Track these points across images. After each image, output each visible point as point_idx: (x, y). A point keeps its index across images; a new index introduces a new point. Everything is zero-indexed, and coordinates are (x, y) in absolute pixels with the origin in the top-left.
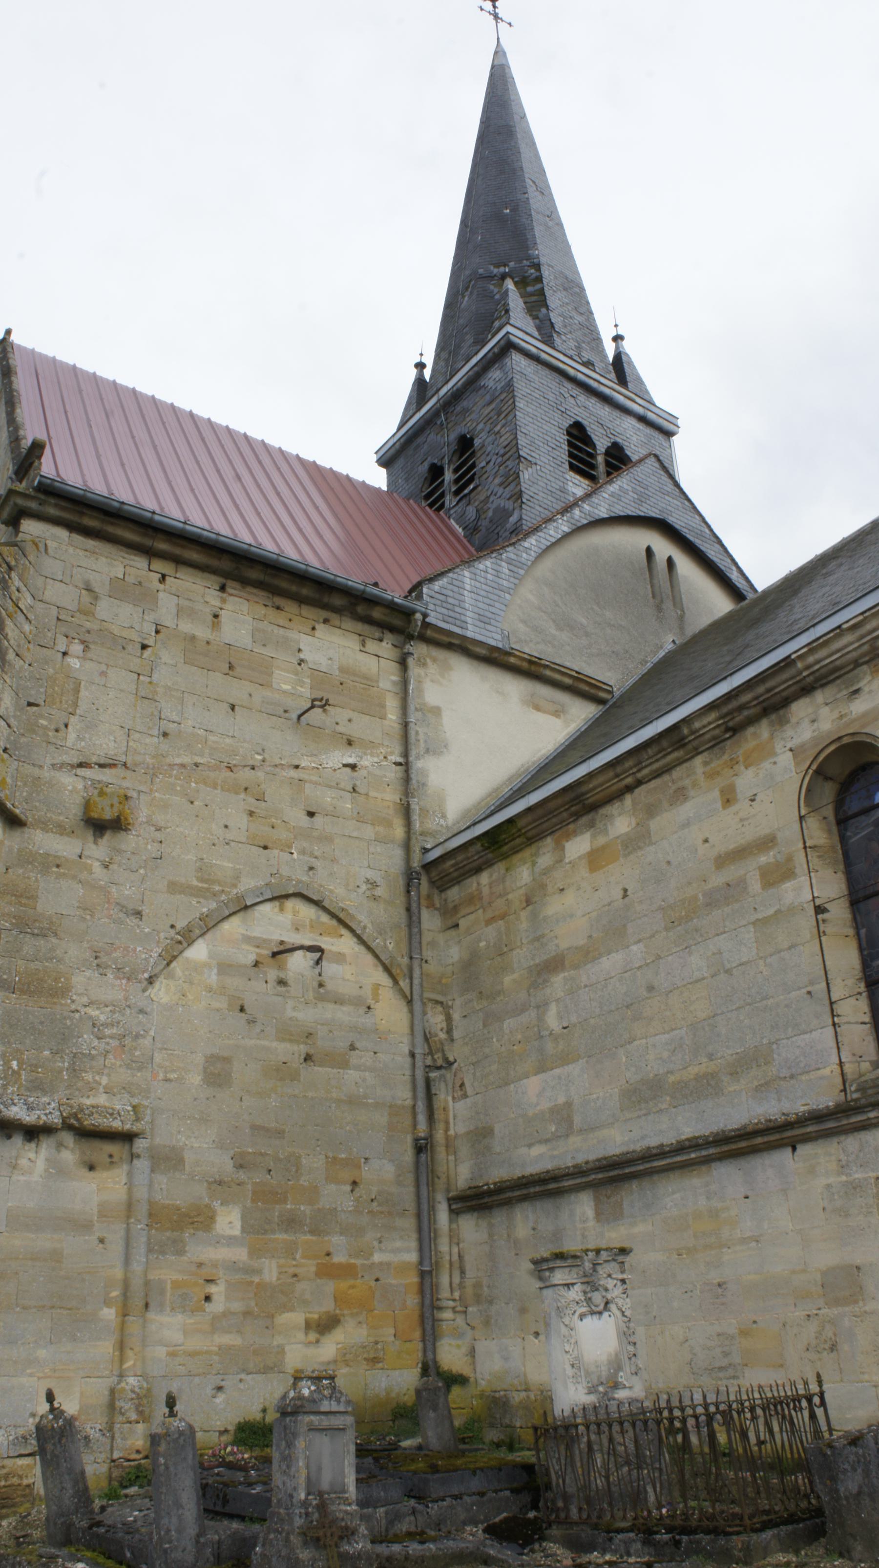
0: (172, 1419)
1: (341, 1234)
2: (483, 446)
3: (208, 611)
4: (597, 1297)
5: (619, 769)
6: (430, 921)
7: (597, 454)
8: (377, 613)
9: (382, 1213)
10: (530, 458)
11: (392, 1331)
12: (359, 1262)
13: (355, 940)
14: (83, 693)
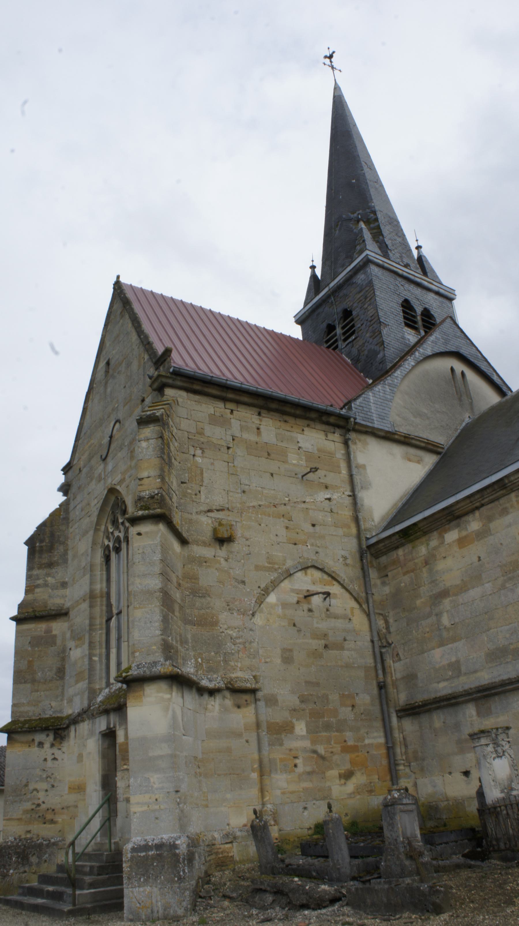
0: (332, 814)
1: (350, 731)
2: (358, 315)
3: (254, 426)
4: (499, 749)
5: (472, 499)
6: (373, 574)
7: (417, 316)
8: (332, 420)
9: (367, 719)
10: (385, 322)
11: (377, 777)
12: (360, 744)
13: (340, 586)
14: (205, 475)
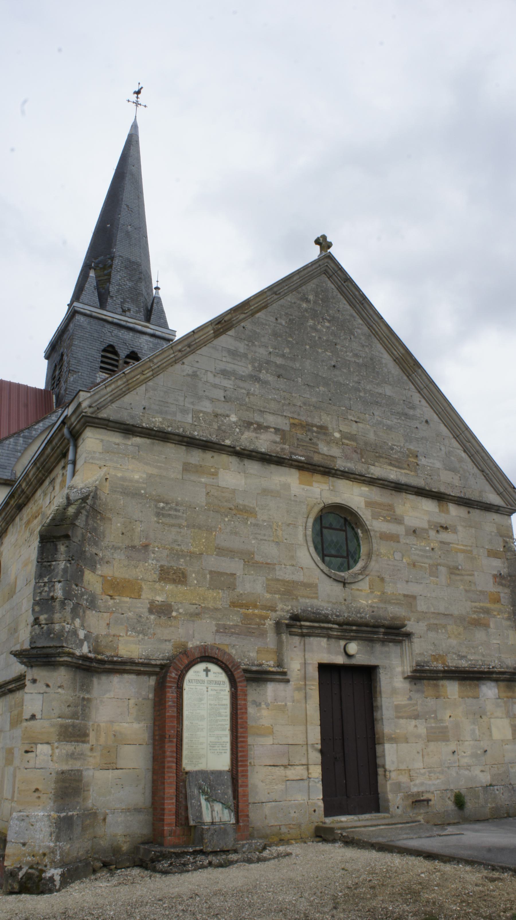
10: (76, 370)
